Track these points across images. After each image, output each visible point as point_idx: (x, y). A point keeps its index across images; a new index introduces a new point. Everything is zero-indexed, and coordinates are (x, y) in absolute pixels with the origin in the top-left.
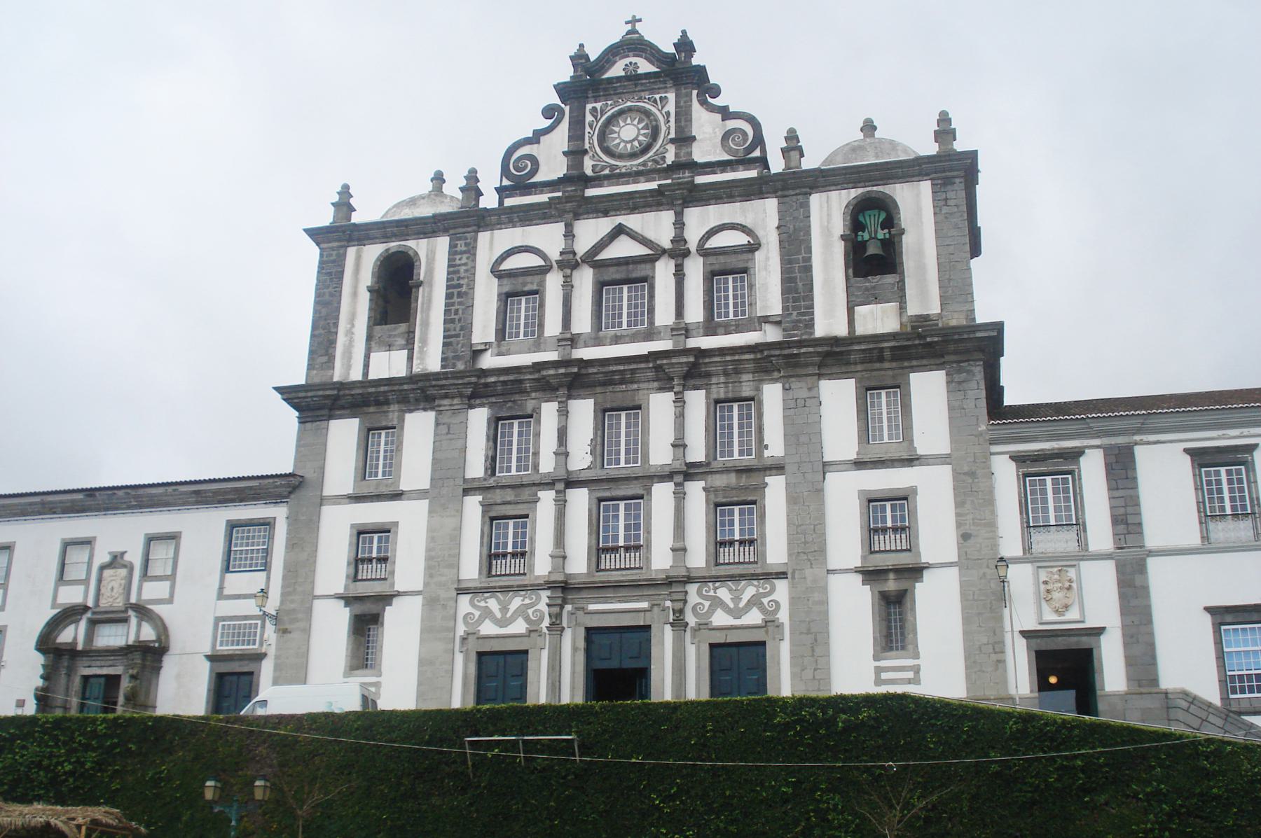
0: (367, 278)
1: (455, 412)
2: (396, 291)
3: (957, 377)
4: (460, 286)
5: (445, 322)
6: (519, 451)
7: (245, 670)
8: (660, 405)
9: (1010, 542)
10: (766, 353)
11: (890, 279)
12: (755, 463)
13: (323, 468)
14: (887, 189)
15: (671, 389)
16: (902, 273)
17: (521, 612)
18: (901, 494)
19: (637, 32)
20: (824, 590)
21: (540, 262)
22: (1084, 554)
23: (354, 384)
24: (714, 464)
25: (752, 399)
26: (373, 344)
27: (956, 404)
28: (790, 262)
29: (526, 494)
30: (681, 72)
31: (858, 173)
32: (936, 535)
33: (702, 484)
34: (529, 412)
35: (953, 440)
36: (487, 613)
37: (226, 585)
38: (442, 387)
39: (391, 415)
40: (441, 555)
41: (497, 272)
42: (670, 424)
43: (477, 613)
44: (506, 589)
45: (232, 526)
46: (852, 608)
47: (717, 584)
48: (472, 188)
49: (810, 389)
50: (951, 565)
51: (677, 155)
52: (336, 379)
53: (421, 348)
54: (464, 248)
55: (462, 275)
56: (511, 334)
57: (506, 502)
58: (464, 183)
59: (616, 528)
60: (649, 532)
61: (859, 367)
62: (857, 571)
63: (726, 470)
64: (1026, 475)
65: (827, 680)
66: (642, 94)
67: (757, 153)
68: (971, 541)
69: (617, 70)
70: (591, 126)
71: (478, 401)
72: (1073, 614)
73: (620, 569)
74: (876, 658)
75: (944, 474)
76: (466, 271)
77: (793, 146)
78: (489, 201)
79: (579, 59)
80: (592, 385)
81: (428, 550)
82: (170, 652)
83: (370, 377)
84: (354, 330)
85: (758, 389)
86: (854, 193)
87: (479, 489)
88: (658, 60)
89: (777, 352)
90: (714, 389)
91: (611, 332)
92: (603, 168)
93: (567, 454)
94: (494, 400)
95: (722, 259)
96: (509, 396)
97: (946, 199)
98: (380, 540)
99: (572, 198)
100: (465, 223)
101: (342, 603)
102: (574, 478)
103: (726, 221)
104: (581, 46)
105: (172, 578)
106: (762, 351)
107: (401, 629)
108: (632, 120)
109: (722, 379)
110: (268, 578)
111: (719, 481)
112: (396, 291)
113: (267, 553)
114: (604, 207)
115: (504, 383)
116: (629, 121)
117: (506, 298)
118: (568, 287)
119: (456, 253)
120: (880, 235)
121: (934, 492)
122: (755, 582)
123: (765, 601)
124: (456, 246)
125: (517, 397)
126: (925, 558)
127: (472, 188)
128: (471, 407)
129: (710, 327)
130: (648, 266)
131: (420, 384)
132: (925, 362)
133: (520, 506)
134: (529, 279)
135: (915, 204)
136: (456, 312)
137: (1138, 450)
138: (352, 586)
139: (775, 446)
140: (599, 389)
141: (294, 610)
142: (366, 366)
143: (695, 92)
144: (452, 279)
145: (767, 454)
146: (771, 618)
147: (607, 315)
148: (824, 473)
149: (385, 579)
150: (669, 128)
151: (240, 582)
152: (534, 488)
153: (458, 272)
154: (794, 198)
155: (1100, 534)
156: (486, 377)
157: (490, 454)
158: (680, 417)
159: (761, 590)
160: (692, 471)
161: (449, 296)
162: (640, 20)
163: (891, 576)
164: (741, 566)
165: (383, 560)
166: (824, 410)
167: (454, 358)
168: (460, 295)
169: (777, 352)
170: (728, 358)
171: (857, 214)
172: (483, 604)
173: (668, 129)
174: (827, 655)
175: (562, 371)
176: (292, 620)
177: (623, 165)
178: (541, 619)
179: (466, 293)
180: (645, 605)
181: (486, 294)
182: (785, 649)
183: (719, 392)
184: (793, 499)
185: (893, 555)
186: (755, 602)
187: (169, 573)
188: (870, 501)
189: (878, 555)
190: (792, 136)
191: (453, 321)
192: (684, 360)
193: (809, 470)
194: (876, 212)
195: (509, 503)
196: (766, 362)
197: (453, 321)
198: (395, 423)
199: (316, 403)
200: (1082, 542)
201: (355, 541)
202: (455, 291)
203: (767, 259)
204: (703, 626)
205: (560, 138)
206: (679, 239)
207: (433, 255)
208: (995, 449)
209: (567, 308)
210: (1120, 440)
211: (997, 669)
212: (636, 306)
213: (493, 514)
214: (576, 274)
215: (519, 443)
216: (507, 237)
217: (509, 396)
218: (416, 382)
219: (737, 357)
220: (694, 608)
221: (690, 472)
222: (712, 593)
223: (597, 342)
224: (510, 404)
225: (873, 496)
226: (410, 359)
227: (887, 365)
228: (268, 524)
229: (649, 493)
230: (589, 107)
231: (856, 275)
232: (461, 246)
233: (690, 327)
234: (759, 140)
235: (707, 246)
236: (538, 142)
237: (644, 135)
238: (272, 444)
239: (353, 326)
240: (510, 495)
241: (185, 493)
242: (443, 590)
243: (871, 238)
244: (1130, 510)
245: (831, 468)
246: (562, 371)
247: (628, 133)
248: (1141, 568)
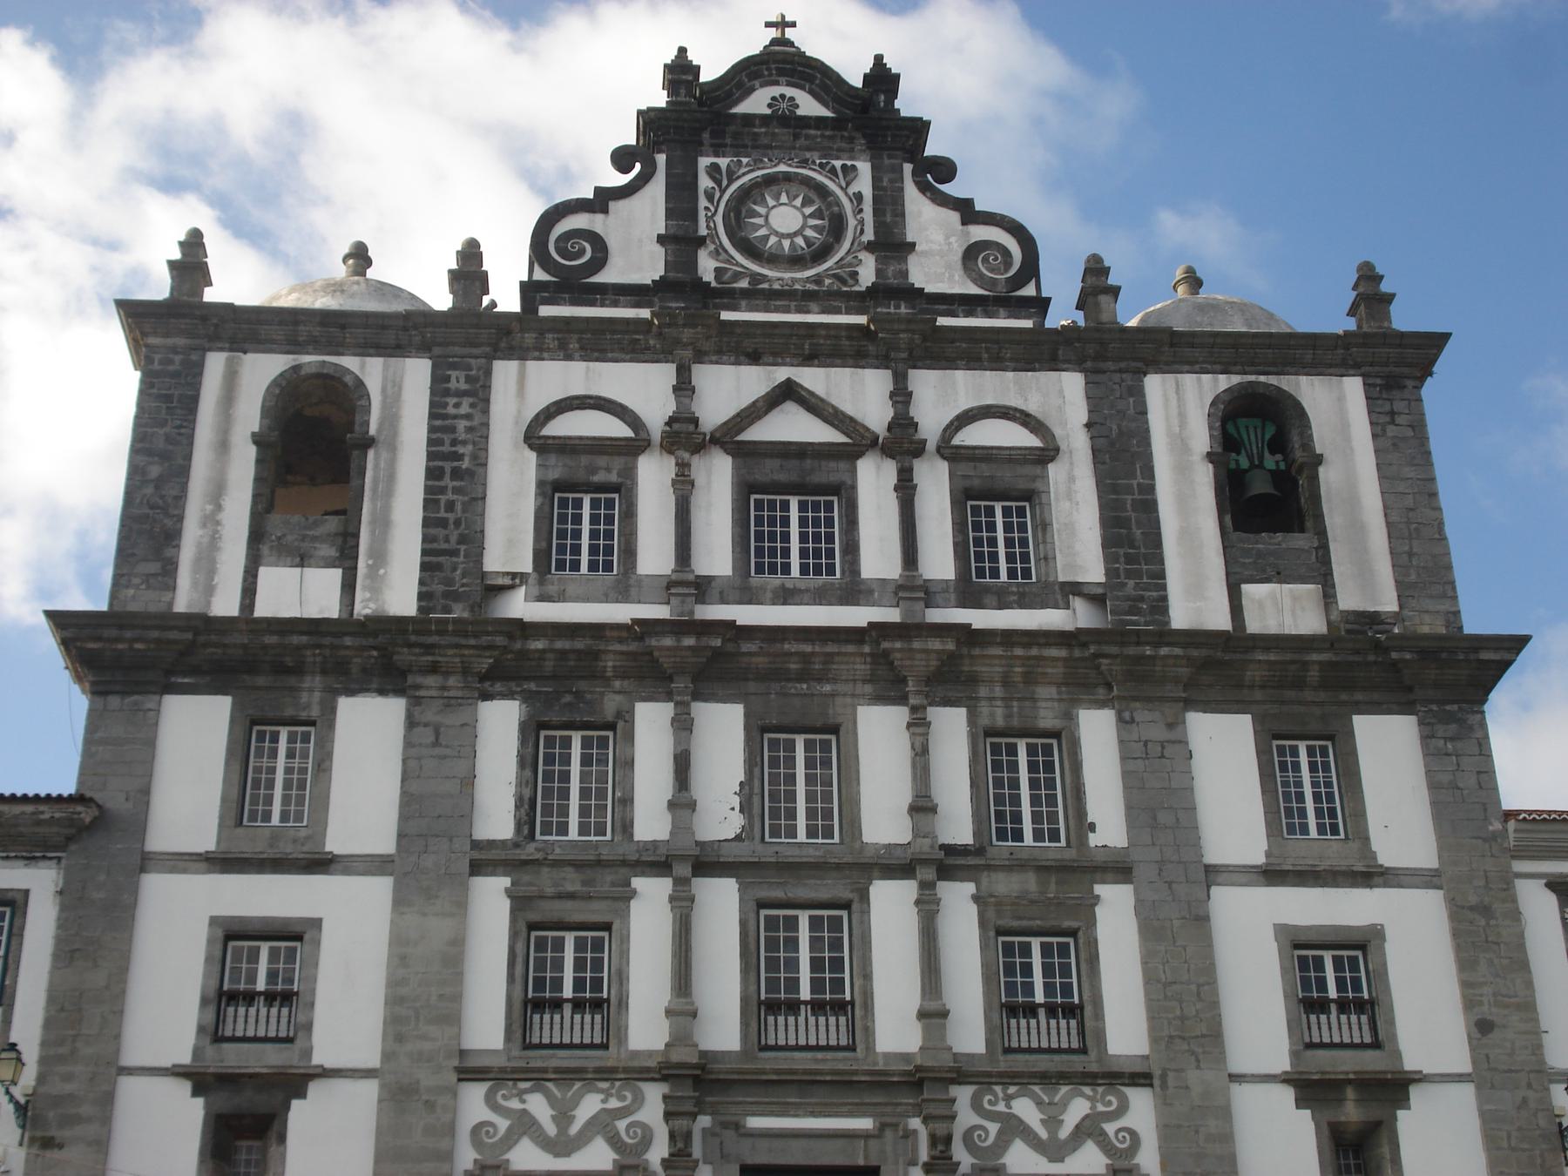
0: (250, 416)
1: (450, 704)
2: (314, 452)
4: (460, 457)
5: (426, 523)
6: (585, 793)
8: (879, 732)
11: (1299, 541)
12: (1071, 854)
13: (146, 792)
14: (1285, 382)
15: (901, 700)
16: (1322, 533)
20: (1225, 1113)
24: (991, 852)
25: (1056, 735)
26: (265, 550)
27: (1445, 778)
29: (609, 877)
33: (970, 888)
34: (610, 718)
35: (1442, 849)
36: (525, 1125)
40: (421, 995)
41: (533, 438)
43: (503, 1124)
44: (1049, 1079)
47: (1012, 1090)
48: (469, 272)
50: (368, 1073)
51: (879, 272)
53: (373, 570)
54: (463, 386)
55: (462, 436)
57: (569, 894)
58: (176, 255)
60: (867, 976)
62: (1285, 1079)
63: (1018, 865)
66: (808, 155)
67: (1029, 291)
68: (1496, 1035)
69: (757, 103)
70: (710, 196)
71: (498, 687)
73: (571, 1046)
76: (470, 429)
77: (1097, 283)
79: (680, 72)
81: (393, 983)
84: (222, 516)
85: (1070, 717)
86: (1224, 382)
88: (834, 100)
89: (1114, 650)
92: (737, 276)
93: (692, 806)
94: (532, 686)
95: (985, 469)
97: (1392, 413)
99: (684, 317)
100: (463, 339)
103: (989, 401)
108: (792, 198)
111: (1005, 885)
112: (314, 452)
114: (749, 347)
115: (563, 654)
116: (784, 199)
118: (684, 488)
120: (1270, 462)
121: (353, 926)
122: (1087, 1090)
123: (1110, 1128)
124: (448, 379)
125: (582, 685)
126: (1410, 1063)
127: (469, 272)
128: (487, 697)
129: (969, 594)
130: (843, 465)
132: (1376, 696)
133: (595, 905)
134: (602, 461)
135: (1336, 410)
136: (450, 506)
138: (210, 1051)
139: (1109, 826)
140: (752, 686)
141: (71, 1098)
143: (908, 168)
144: (440, 442)
145: (1094, 840)
146: (631, 1161)
148: (1209, 887)
149: (289, 1040)
150: (862, 222)
152: (624, 871)
153: (453, 429)
154: (1116, 378)
157: (527, 793)
159: (1101, 1108)
160: (951, 861)
161: (432, 474)
162: (793, 25)
163: (1350, 1093)
167: (446, 595)
168: (457, 474)
169: (1114, 650)
172: (514, 1104)
173: (862, 224)
175: (689, 641)
178: (646, 1141)
179: (470, 473)
180: (865, 1123)
183: (997, 715)
184: (1151, 928)
186: (602, 1125)
188: (229, 937)
189: (1321, 1053)
190: (1096, 270)
191: (443, 523)
192: (935, 644)
194: (1258, 422)
195: (572, 896)
197: (443, 523)
198: (315, 712)
199: (124, 652)
201: (218, 953)
202: (448, 466)
203: (1072, 479)
205: (648, 212)
206: (903, 424)
207: (400, 394)
208: (1520, 866)
209: (684, 524)
213: (534, 917)
217: (572, 687)
218: (375, 634)
219: (1034, 652)
220: (476, 1130)
221: (951, 863)
222: (1001, 1107)
223: (749, 596)
224: (568, 698)
226: (349, 586)
227: (1308, 695)
229: (864, 897)
230: (704, 162)
231: (1238, 527)
234: (1030, 268)
235: (956, 441)
236: (605, 211)
237: (814, 228)
239: (219, 508)
240: (572, 881)
243: (1253, 466)
245: (1220, 878)
247: (785, 219)
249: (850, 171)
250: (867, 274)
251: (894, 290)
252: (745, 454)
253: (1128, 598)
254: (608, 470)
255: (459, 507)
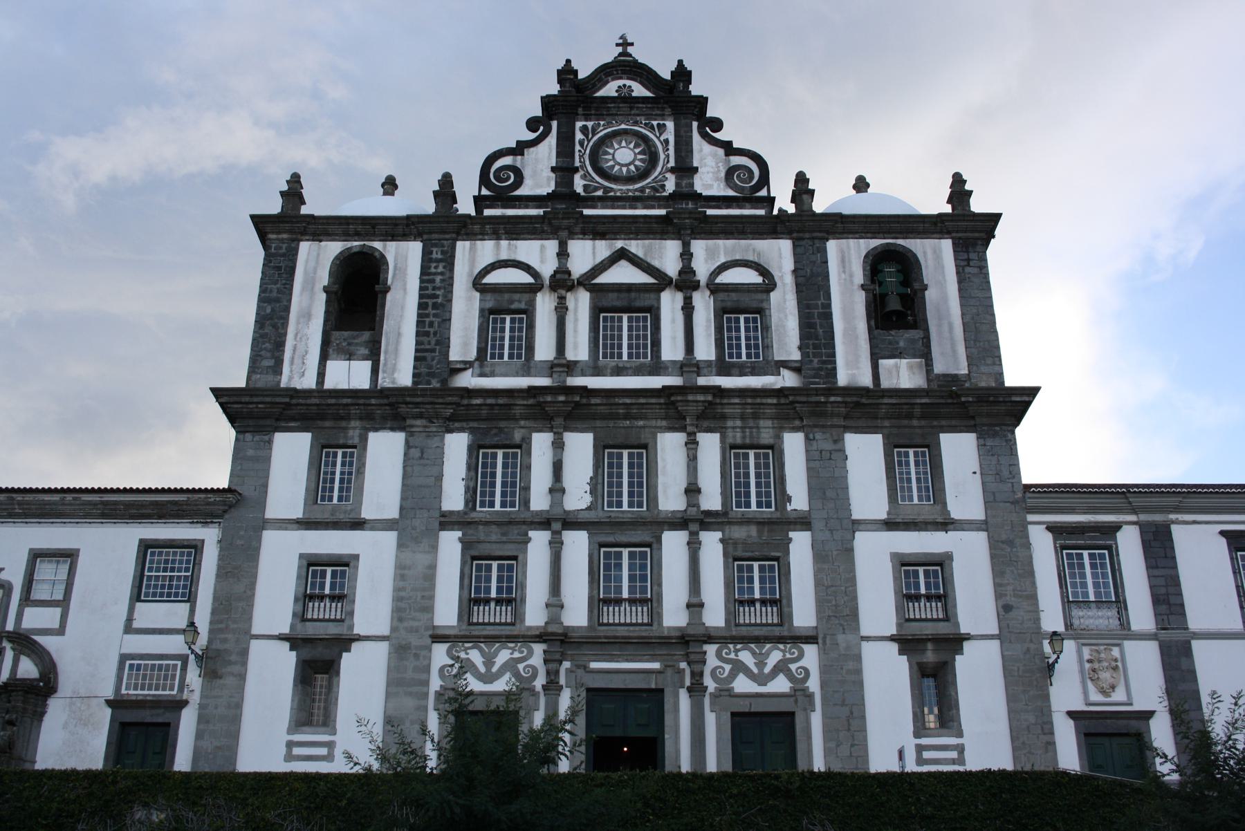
1: (429, 435)
3: (989, 442)
5: (418, 334)
6: (631, 485)
7: (160, 720)
8: (670, 445)
9: (1052, 618)
10: (791, 398)
14: (377, 245)
15: (682, 429)
16: (927, 330)
17: (510, 666)
18: (937, 560)
19: (630, 55)
20: (858, 658)
21: (528, 279)
22: (1125, 631)
23: (307, 393)
25: (771, 447)
28: (808, 307)
29: (514, 532)
30: (677, 98)
31: (879, 223)
32: (975, 604)
36: (739, 667)
37: (136, 615)
38: (417, 404)
39: (351, 433)
40: (412, 596)
41: (477, 283)
42: (685, 466)
44: (491, 639)
45: (146, 546)
46: (887, 677)
47: (739, 646)
49: (835, 442)
50: (991, 637)
51: (677, 185)
52: (283, 385)
54: (439, 256)
56: (493, 357)
57: (494, 541)
59: (619, 579)
61: (887, 423)
62: (892, 638)
64: (1063, 547)
65: (865, 757)
67: (763, 193)
68: (1013, 614)
69: (610, 89)
71: (457, 425)
72: (1119, 695)
74: (290, 731)
75: (979, 540)
78: (465, 206)
79: (566, 73)
80: (594, 417)
81: (397, 590)
82: (56, 695)
83: (328, 384)
85: (779, 438)
87: (459, 523)
89: (803, 399)
90: (730, 433)
91: (612, 363)
94: (475, 425)
95: (734, 296)
96: (498, 423)
98: (334, 574)
99: (562, 215)
100: (440, 228)
101: (287, 645)
102: (571, 518)
104: (568, 61)
105: (64, 603)
106: (786, 396)
107: (362, 679)
109: (738, 423)
110: (192, 611)
111: (738, 533)
113: (193, 580)
114: (597, 230)
116: (624, 144)
117: (490, 316)
118: (561, 311)
119: (431, 260)
121: (375, 555)
122: (781, 646)
123: (793, 667)
125: (502, 424)
127: (445, 193)
129: (723, 368)
130: (653, 296)
131: (392, 400)
132: (954, 422)
134: (517, 296)
135: (937, 258)
136: (431, 324)
137: (1174, 528)
138: (299, 626)
139: (799, 500)
140: (598, 423)
142: (321, 375)
143: (695, 124)
147: (605, 346)
150: (668, 156)
151: (151, 613)
152: (524, 527)
153: (433, 281)
155: (1141, 613)
156: (470, 398)
158: (692, 460)
159: (788, 656)
161: (421, 306)
163: (930, 646)
164: (637, 628)
165: (337, 598)
166: (850, 464)
167: (429, 374)
168: (435, 306)
169: (803, 399)
170: (749, 401)
171: (875, 263)
173: (668, 157)
174: (863, 729)
175: (562, 398)
176: (222, 660)
177: (618, 188)
179: (442, 305)
180: (656, 665)
181: (465, 312)
182: (816, 720)
183: (738, 438)
184: (820, 556)
185: (930, 624)
186: (781, 668)
187: (60, 597)
188: (310, 565)
191: (427, 334)
192: (700, 398)
193: (835, 527)
196: (792, 408)
197: (427, 334)
198: (356, 441)
200: (1124, 623)
202: (430, 302)
204: (725, 692)
205: (545, 154)
206: (687, 270)
207: (404, 260)
209: (564, 333)
210: (1158, 518)
211: (1047, 752)
212: (638, 337)
214: (570, 299)
215: (504, 475)
216: (487, 251)
217: (498, 423)
219: (758, 401)
222: (732, 656)
223: (597, 371)
225: (907, 560)
226: (375, 371)
227: (915, 422)
228: (195, 547)
230: (579, 124)
232: (437, 254)
233: (702, 365)
234: (765, 180)
235: (718, 280)
237: (641, 160)
238: (201, 454)
241: (89, 503)
242: (410, 637)
244: (1171, 590)
246: (562, 398)
247: (624, 155)
248: (1187, 651)
249: (662, 128)
250: (670, 185)
251: (686, 195)
252: (598, 291)
253: (814, 369)
254: (520, 301)
255: (436, 324)
